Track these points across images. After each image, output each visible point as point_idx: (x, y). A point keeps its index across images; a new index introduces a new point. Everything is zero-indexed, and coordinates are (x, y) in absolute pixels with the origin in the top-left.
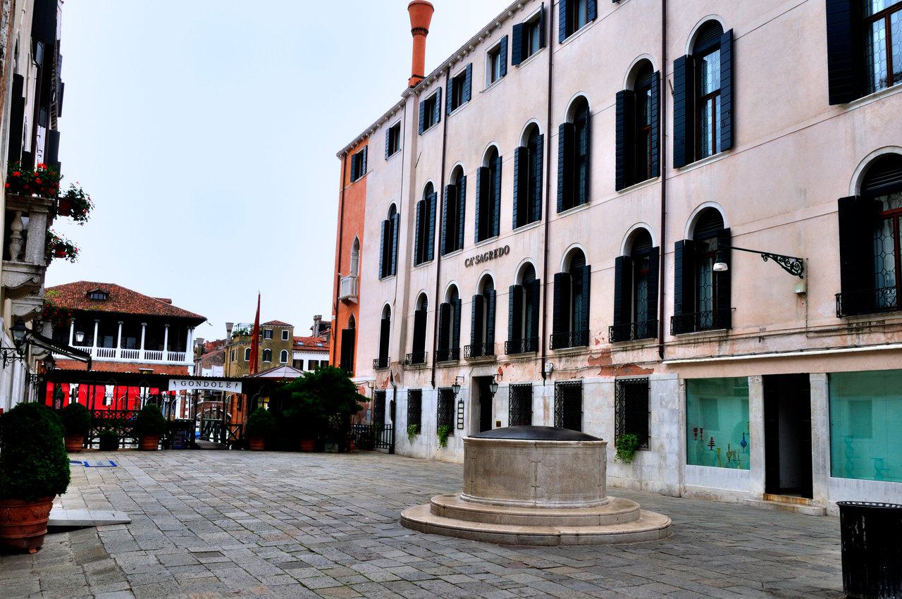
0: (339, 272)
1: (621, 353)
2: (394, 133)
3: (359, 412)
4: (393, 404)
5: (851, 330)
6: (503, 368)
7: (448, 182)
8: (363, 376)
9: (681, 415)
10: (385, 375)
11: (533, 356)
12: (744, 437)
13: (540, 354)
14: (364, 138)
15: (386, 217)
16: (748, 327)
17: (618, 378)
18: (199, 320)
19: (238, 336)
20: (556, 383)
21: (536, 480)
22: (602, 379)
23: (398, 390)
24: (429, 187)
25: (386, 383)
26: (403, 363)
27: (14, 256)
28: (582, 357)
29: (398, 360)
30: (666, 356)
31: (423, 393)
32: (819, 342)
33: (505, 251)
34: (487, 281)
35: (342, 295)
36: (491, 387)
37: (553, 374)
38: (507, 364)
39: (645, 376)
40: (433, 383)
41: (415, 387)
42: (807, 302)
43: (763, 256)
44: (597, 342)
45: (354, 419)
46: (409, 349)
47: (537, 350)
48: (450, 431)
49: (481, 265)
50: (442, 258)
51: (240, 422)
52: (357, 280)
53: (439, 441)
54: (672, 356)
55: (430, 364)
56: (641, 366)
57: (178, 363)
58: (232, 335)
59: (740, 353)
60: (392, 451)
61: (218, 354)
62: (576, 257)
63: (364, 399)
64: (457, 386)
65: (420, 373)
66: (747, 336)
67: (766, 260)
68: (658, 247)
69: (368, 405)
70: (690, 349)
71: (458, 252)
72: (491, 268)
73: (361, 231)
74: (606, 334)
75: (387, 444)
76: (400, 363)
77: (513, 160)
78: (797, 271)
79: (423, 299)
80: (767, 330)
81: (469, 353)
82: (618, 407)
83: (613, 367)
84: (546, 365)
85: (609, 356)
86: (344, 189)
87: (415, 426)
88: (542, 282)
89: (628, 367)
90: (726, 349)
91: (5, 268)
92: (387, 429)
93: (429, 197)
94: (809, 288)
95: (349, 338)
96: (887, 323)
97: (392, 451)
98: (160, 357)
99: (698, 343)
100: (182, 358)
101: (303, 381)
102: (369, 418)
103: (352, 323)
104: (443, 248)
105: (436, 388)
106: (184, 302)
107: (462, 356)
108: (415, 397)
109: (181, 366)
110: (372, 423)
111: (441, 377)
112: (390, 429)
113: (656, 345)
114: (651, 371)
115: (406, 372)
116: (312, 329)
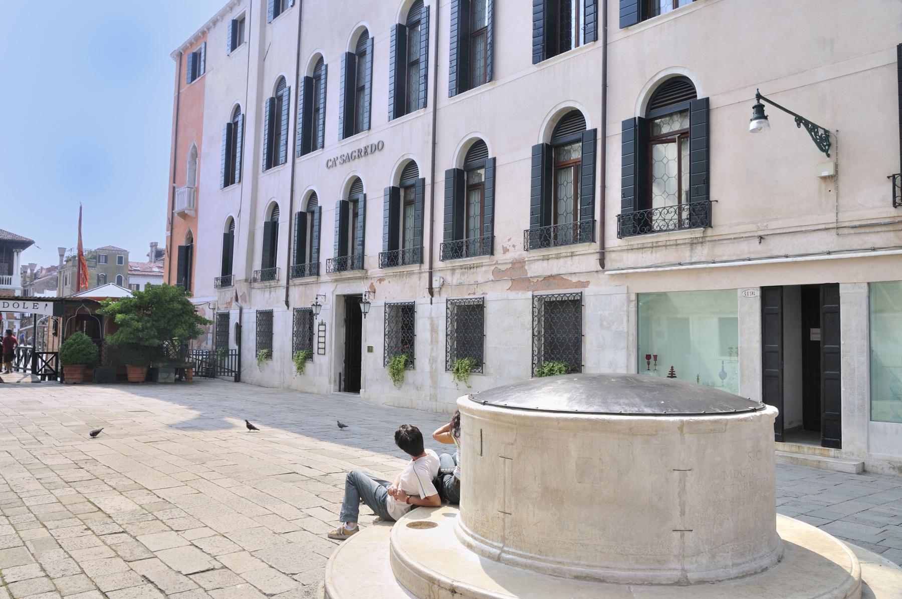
0: (174, 182)
1: (540, 263)
2: (237, 27)
3: (200, 337)
4: (239, 327)
6: (376, 285)
7: (304, 73)
8: (203, 297)
9: (631, 338)
10: (229, 293)
11: (415, 268)
12: (723, 367)
13: (426, 266)
14: (203, 34)
15: (228, 119)
16: (738, 224)
17: (536, 293)
18: (24, 244)
19: (71, 260)
20: (447, 301)
21: (683, 513)
22: (512, 295)
23: (244, 311)
24: (282, 81)
25: (230, 303)
26: (250, 281)
28: (484, 269)
29: (244, 278)
31: (275, 314)
32: (855, 241)
33: (379, 147)
34: (356, 183)
35: (178, 208)
36: (362, 306)
37: (443, 290)
38: (381, 280)
39: (578, 290)
40: (287, 303)
41: (466, 295)
42: (837, 188)
43: (796, 120)
44: (506, 250)
45: (194, 344)
46: (258, 265)
47: (422, 262)
48: (309, 356)
49: (347, 165)
50: (297, 161)
51: (56, 350)
52: (194, 192)
53: (295, 368)
54: (616, 265)
55: (283, 281)
56: (570, 279)
58: (65, 259)
59: (725, 258)
60: (238, 379)
61: (52, 279)
62: (476, 148)
63: (205, 322)
64: (317, 305)
65: (270, 292)
66: (737, 236)
67: (799, 125)
68: (595, 131)
69: (209, 328)
70: (644, 255)
71: (318, 152)
72: (359, 168)
73: (200, 139)
74: (519, 240)
75: (232, 371)
76: (246, 280)
77: (389, 39)
79: (275, 208)
80: (770, 228)
81: (332, 267)
82: (449, 329)
83: (528, 280)
84: (434, 279)
85: (523, 267)
86: (179, 93)
87: (265, 351)
88: (428, 181)
89: (550, 279)
90: (702, 253)
92: (232, 355)
93: (280, 93)
94: (840, 170)
95: (186, 255)
97: (238, 379)
99: (659, 246)
100: (9, 282)
101: (131, 301)
102: (210, 342)
103: (191, 239)
104: (298, 148)
105: (291, 308)
107: (323, 270)
108: (266, 319)
109: (7, 290)
110: (214, 347)
111: (297, 296)
112: (235, 355)
113: (592, 251)
114: (586, 284)
115: (254, 291)
116: (148, 255)
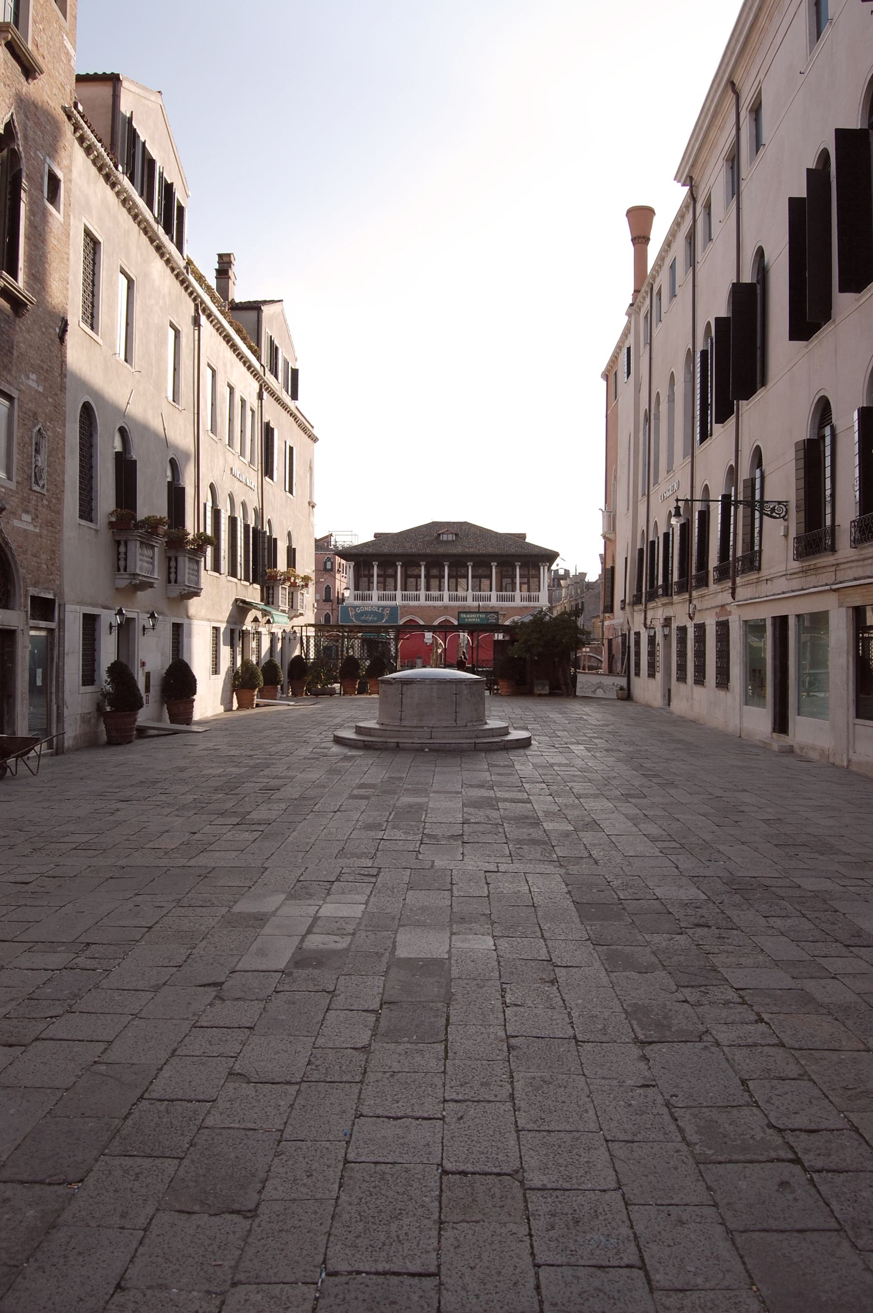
5: (805, 572)
27: (122, 568)
30: (737, 597)
57: (532, 604)
78: (779, 514)
91: (117, 577)
96: (818, 565)
98: (512, 599)
106: (537, 538)
